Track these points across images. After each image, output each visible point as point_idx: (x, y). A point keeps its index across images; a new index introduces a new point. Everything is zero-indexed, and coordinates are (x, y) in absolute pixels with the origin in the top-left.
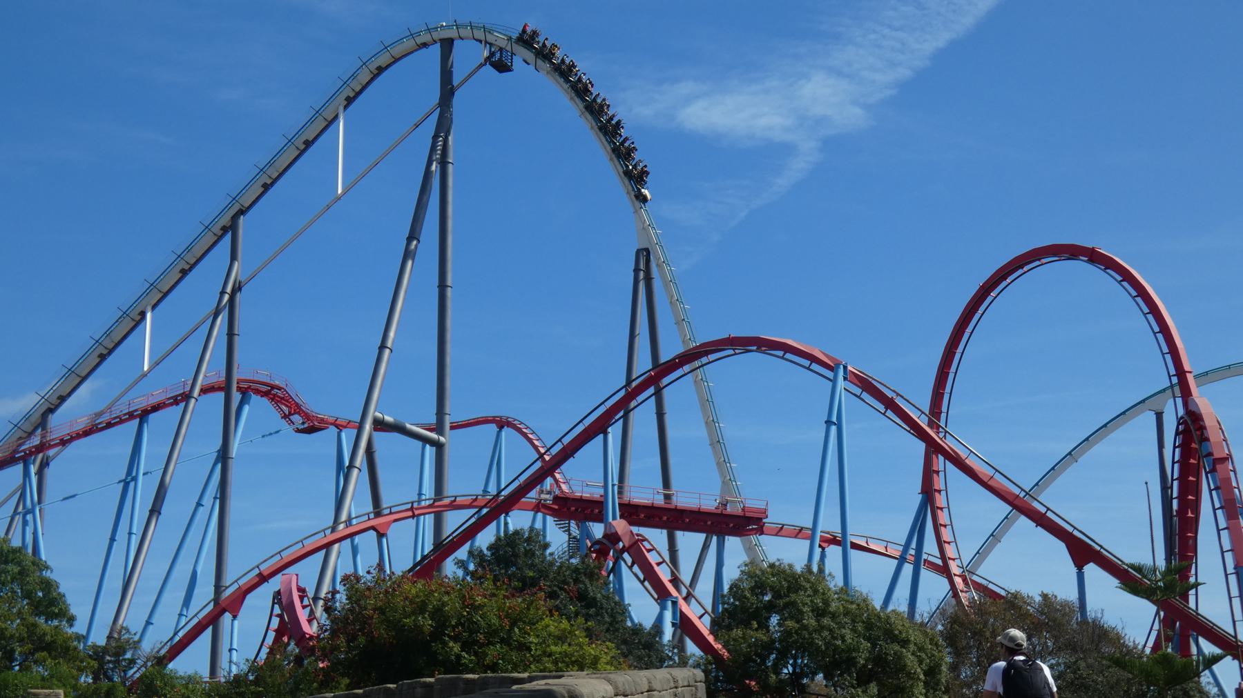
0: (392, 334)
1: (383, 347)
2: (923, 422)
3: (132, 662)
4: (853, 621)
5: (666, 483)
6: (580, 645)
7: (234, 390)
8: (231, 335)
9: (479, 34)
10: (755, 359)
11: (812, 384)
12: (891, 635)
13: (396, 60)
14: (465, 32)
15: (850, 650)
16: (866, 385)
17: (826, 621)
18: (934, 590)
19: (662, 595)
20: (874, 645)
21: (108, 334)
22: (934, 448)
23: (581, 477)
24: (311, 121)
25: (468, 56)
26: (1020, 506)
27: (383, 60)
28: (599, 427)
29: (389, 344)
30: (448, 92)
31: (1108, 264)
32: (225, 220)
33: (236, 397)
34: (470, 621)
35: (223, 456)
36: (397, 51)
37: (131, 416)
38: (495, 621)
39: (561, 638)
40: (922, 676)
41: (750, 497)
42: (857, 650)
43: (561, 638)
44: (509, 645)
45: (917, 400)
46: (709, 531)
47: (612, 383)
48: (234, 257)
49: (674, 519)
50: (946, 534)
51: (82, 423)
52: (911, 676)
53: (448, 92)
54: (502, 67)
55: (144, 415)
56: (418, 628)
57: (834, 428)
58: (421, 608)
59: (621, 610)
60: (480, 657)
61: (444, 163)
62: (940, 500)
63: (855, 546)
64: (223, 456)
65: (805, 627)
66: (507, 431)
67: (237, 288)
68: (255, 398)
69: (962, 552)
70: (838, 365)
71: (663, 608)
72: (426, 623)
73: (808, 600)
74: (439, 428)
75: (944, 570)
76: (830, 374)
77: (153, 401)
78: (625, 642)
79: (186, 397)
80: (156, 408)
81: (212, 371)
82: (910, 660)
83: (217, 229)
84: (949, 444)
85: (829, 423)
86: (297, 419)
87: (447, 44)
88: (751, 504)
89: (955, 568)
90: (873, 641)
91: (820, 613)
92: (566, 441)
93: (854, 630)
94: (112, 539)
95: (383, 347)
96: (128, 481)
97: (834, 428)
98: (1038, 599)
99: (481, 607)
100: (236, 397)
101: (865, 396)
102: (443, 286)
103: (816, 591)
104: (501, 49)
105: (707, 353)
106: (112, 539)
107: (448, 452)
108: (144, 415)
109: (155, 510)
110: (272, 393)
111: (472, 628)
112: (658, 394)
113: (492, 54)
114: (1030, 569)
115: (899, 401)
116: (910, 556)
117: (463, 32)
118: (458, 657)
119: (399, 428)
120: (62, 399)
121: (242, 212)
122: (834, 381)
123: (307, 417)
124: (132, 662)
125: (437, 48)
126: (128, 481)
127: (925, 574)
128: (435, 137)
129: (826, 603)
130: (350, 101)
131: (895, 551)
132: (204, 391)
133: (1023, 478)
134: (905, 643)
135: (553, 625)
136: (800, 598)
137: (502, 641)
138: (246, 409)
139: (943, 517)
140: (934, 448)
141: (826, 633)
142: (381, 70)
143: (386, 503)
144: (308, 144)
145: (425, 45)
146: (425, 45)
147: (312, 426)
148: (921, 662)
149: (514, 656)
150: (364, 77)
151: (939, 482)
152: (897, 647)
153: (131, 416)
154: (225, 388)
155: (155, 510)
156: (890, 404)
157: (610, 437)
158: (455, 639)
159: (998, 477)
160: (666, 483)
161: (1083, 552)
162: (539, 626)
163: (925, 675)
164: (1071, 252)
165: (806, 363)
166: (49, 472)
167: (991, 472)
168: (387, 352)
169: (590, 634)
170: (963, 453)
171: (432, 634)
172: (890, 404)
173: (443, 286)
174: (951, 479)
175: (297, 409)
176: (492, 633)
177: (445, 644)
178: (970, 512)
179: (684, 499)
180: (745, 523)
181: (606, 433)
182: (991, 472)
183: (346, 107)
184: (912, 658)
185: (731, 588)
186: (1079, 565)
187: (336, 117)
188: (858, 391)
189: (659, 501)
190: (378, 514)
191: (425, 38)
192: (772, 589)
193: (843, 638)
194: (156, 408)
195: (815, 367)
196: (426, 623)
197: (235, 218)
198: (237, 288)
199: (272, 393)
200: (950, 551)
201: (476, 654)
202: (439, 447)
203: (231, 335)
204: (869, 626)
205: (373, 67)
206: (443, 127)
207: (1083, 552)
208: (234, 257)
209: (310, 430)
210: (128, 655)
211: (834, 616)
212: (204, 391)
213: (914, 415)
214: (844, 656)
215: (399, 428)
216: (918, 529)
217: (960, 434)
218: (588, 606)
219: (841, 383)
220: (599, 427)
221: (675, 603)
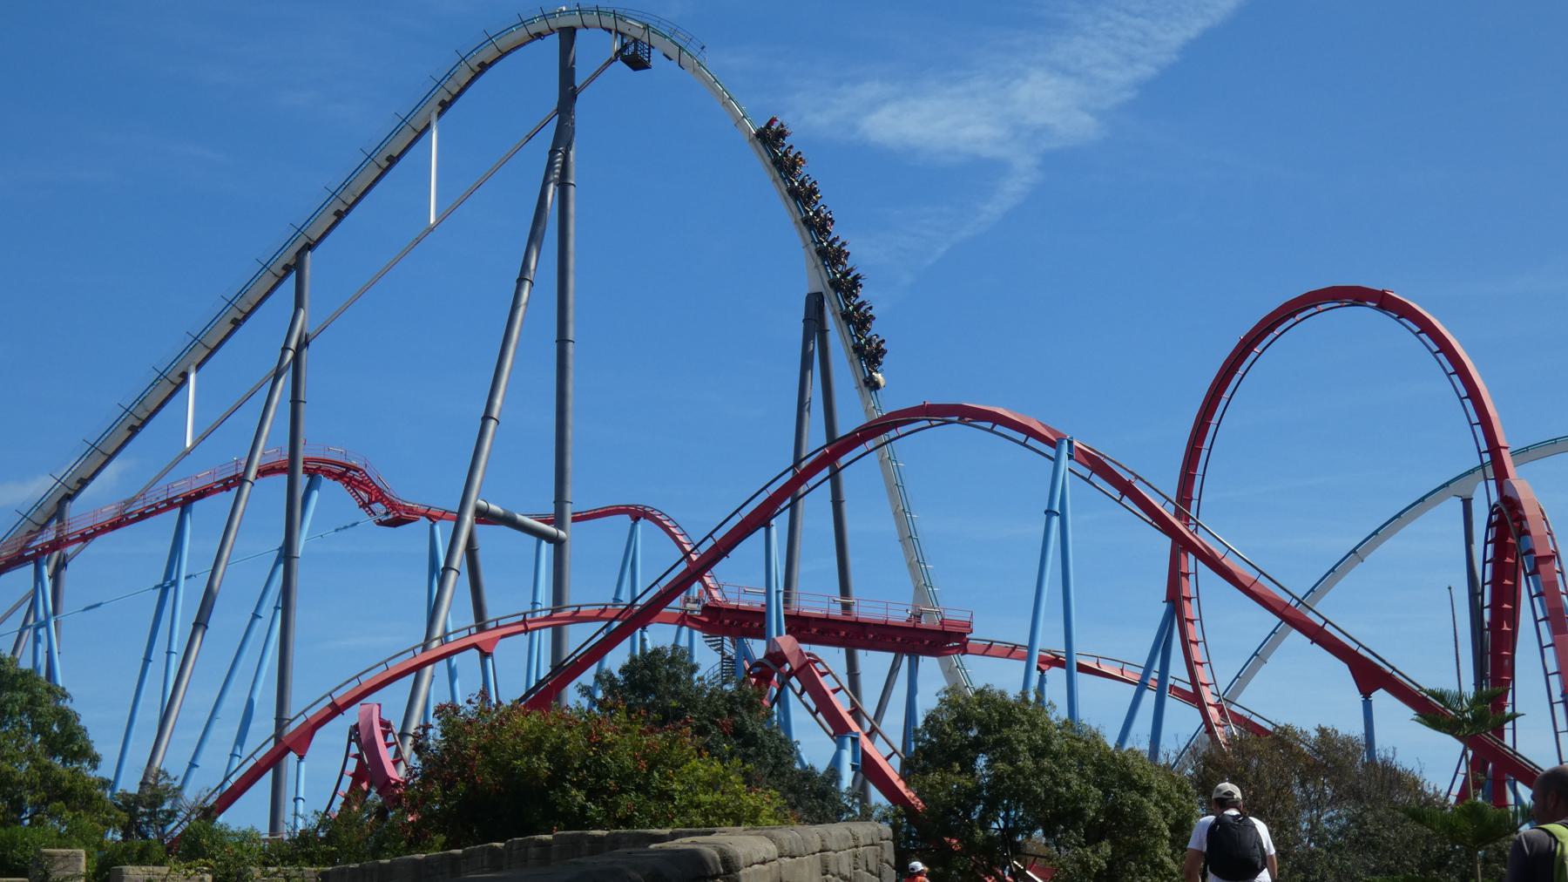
0: (498, 401)
1: (487, 417)
2: (1168, 512)
3: (172, 814)
4: (1081, 763)
5: (845, 590)
6: (736, 794)
7: (300, 472)
8: (295, 401)
9: (608, 22)
10: (956, 432)
11: (1030, 465)
12: (1128, 781)
13: (504, 55)
14: (591, 19)
15: (1076, 799)
16: (1097, 465)
17: (1046, 762)
18: (1182, 723)
19: (839, 729)
20: (1107, 793)
21: (141, 400)
22: (1182, 545)
23: (738, 581)
24: (396, 131)
25: (594, 49)
26: (1292, 617)
27: (487, 55)
28: (760, 519)
29: (495, 414)
30: (568, 95)
31: (1402, 311)
32: (288, 257)
33: (303, 480)
34: (597, 762)
35: (286, 555)
36: (505, 42)
37: (170, 504)
38: (628, 762)
39: (712, 785)
40: (1167, 833)
41: (950, 607)
42: (1085, 799)
43: (712, 785)
44: (647, 793)
45: (1161, 485)
46: (899, 650)
47: (776, 463)
48: (299, 304)
49: (854, 634)
50: (1198, 653)
51: (108, 513)
52: (1153, 832)
53: (568, 95)
54: (637, 63)
55: (187, 503)
56: (532, 772)
57: (1056, 520)
58: (536, 747)
59: (785, 749)
60: (610, 808)
61: (563, 186)
62: (1191, 610)
63: (1083, 669)
64: (286, 555)
65: (1020, 771)
66: (643, 524)
67: (304, 343)
68: (326, 482)
69: (1218, 675)
70: (1061, 439)
71: (841, 746)
72: (543, 766)
73: (1024, 737)
74: (558, 521)
75: (1195, 698)
76: (1051, 452)
77: (198, 485)
78: (792, 789)
79: (240, 480)
80: (201, 494)
81: (272, 447)
82: (1152, 811)
83: (278, 268)
84: (1202, 539)
85: (1050, 513)
86: (379, 508)
87: (568, 35)
88: (951, 615)
89: (1208, 696)
90: (1105, 787)
91: (1038, 753)
92: (718, 536)
93: (1082, 774)
94: (147, 660)
95: (487, 417)
96: (167, 585)
97: (1056, 520)
98: (1314, 734)
99: (611, 745)
100: (303, 480)
101: (1096, 478)
102: (562, 341)
103: (1034, 725)
104: (636, 41)
105: (896, 425)
106: (147, 660)
107: (570, 551)
108: (187, 502)
109: (201, 623)
110: (347, 475)
111: (600, 772)
112: (834, 477)
113: (624, 47)
114: (1305, 697)
115: (1139, 486)
116: (1153, 681)
117: (588, 19)
118: (583, 808)
119: (509, 521)
120: (83, 483)
121: (309, 247)
122: (1056, 461)
123: (392, 505)
124: (172, 814)
125: (554, 40)
126: (167, 585)
127: (1172, 703)
128: (553, 152)
129: (1047, 740)
130: (445, 106)
131: (1134, 674)
132: (262, 473)
133: (1294, 583)
134: (1146, 790)
135: (702, 768)
136: (1017, 733)
137: (638, 788)
138: (315, 495)
139: (1194, 632)
140: (1182, 545)
141: (1046, 778)
142: (484, 67)
143: (490, 615)
144: (393, 160)
145: (540, 35)
146: (540, 35)
147: (399, 518)
148: (1166, 814)
149: (653, 807)
150: (464, 75)
151: (1188, 588)
152: (1135, 796)
153: (170, 504)
154: (289, 469)
155: (201, 623)
156: (1127, 489)
157: (774, 531)
158: (579, 785)
159: (1263, 580)
160: (845, 590)
161: (1370, 676)
162: (685, 769)
163: (1171, 830)
164: (1356, 296)
165: (1021, 437)
166: (66, 575)
167: (1254, 574)
168: (493, 423)
169: (748, 779)
170: (1219, 551)
171: (550, 779)
172: (1127, 489)
173: (562, 341)
174: (1205, 584)
175: (378, 495)
176: (625, 778)
177: (565, 792)
178: (1228, 625)
179: (868, 609)
180: (945, 640)
181: (768, 527)
182: (1254, 574)
183: (440, 114)
184: (1154, 809)
185: (927, 721)
186: (1366, 691)
187: (428, 127)
188: (1086, 472)
189: (836, 611)
190: (481, 628)
191: (540, 26)
192: (979, 723)
193: (1068, 785)
194: (201, 494)
195: (1032, 442)
196: (543, 766)
197: (300, 254)
198: (304, 343)
199: (347, 475)
200: (1203, 674)
201: (605, 804)
202: (558, 543)
203: (295, 401)
204: (1100, 769)
205: (474, 63)
206: (563, 139)
207: (1370, 676)
208: (299, 304)
209: (397, 522)
210: (167, 806)
211: (1056, 757)
212: (262, 473)
213: (1157, 502)
214: (1070, 807)
215: (509, 521)
216: (1162, 646)
217: (1216, 526)
218: (746, 744)
219: (1065, 463)
220: (760, 519)
221: (855, 741)
